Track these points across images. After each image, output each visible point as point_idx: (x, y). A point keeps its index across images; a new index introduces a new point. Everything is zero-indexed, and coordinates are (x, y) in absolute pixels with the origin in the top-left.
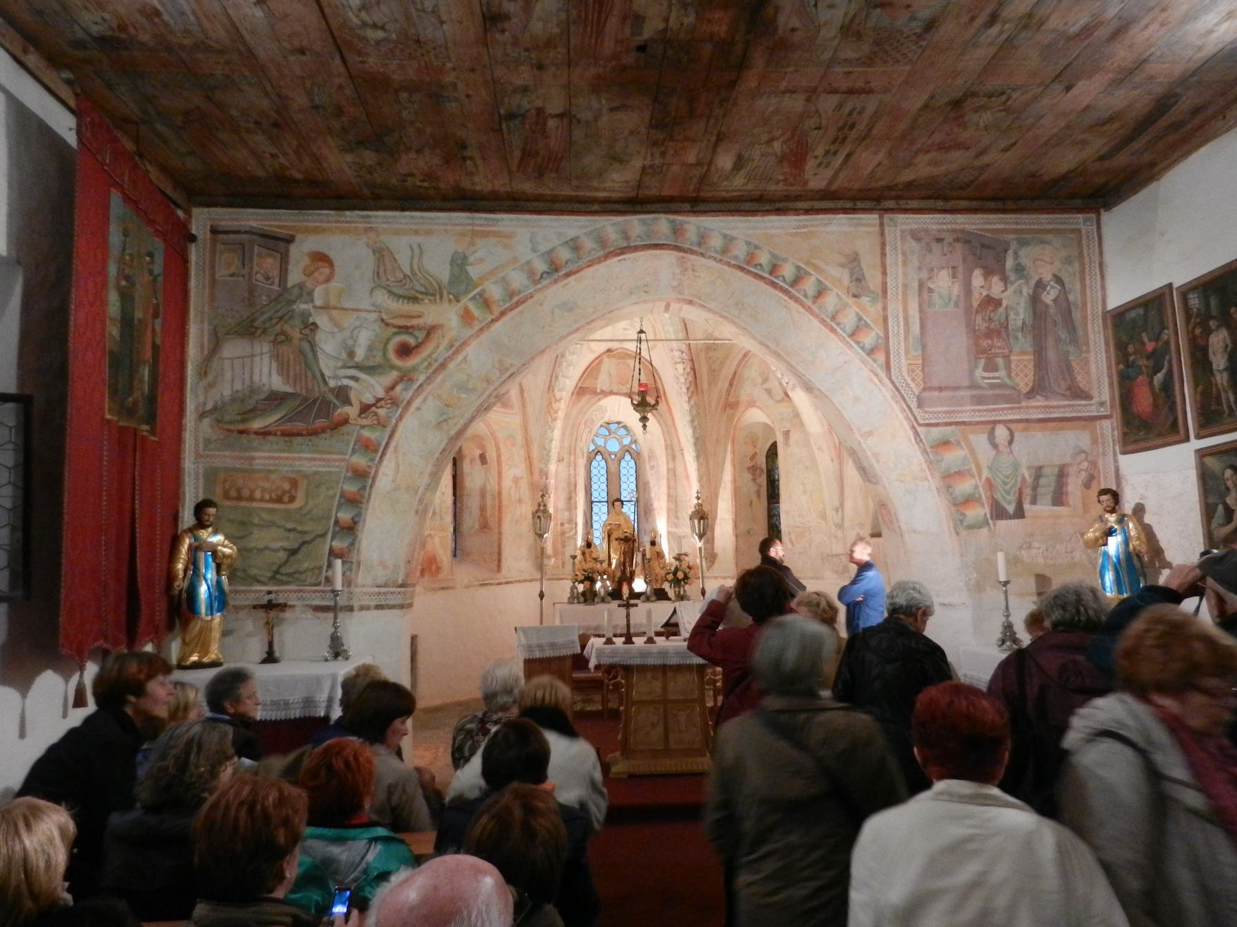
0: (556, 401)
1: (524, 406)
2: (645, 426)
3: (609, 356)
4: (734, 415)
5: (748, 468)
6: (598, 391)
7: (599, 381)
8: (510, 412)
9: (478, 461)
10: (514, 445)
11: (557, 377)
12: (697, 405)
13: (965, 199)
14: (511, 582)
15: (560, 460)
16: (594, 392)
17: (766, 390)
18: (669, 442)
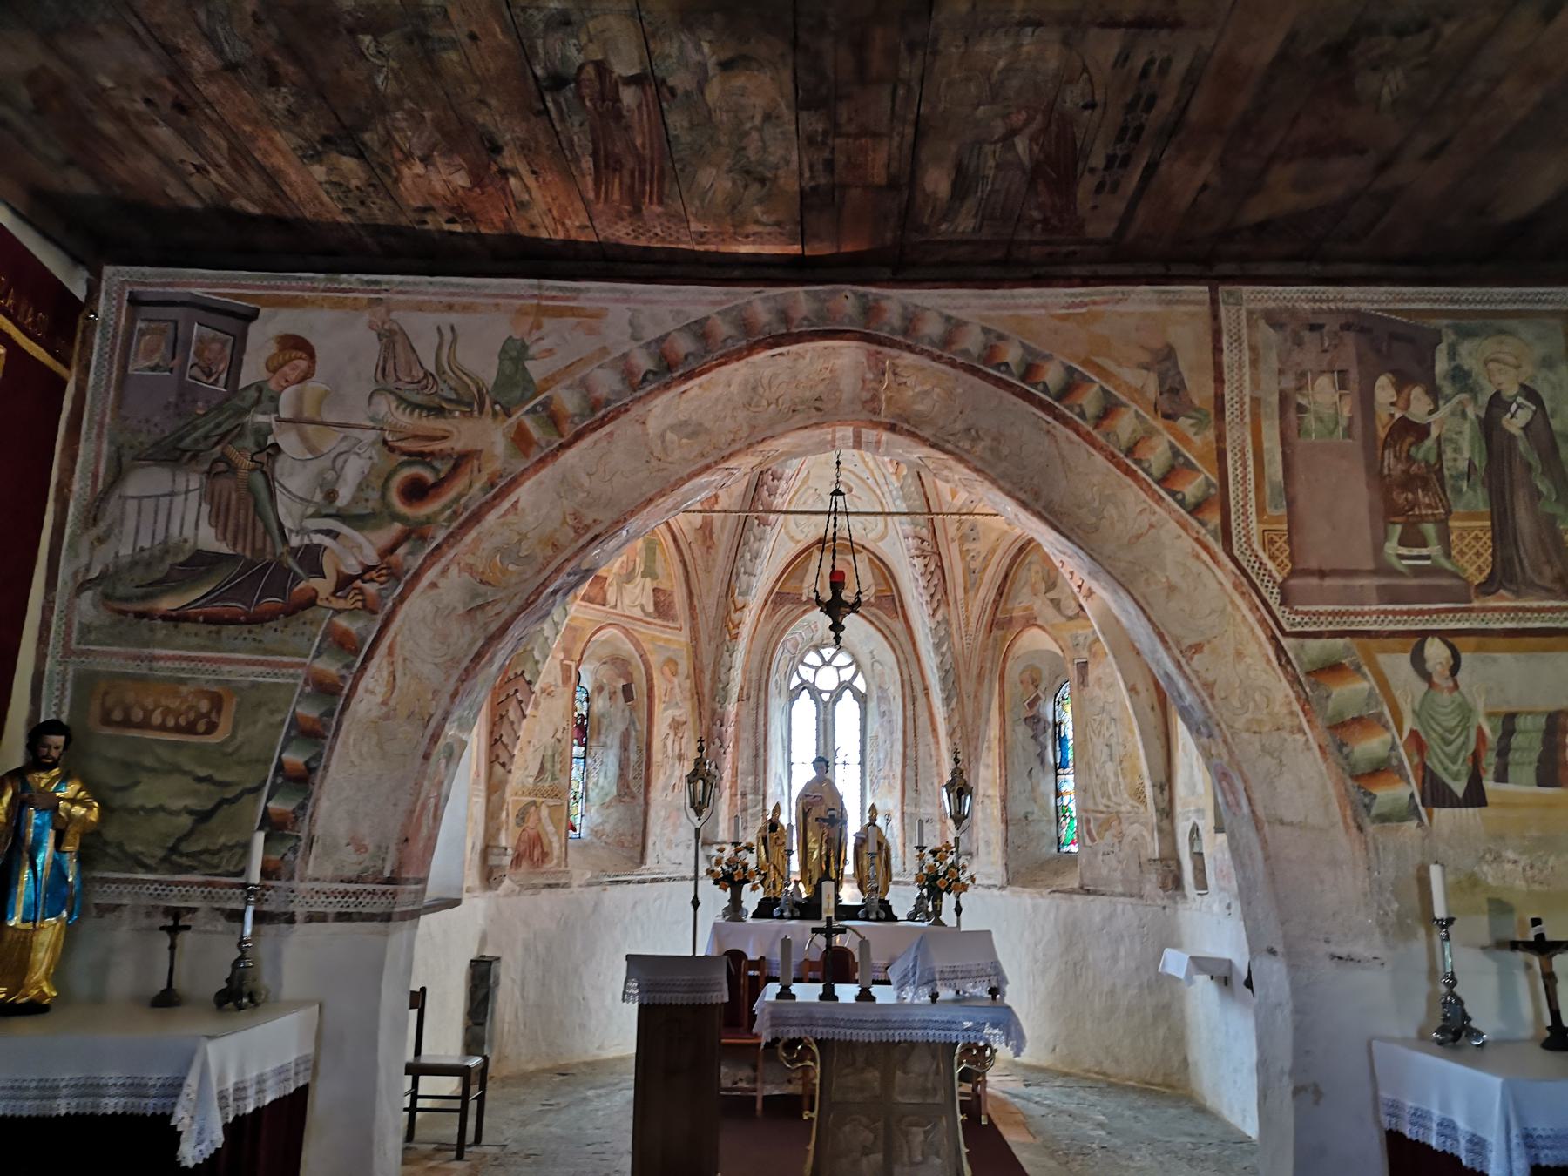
0: (736, 610)
1: (693, 617)
4: (1004, 639)
5: (1026, 719)
6: (804, 599)
8: (671, 625)
10: (674, 674)
17: (1052, 600)
18: (906, 677)
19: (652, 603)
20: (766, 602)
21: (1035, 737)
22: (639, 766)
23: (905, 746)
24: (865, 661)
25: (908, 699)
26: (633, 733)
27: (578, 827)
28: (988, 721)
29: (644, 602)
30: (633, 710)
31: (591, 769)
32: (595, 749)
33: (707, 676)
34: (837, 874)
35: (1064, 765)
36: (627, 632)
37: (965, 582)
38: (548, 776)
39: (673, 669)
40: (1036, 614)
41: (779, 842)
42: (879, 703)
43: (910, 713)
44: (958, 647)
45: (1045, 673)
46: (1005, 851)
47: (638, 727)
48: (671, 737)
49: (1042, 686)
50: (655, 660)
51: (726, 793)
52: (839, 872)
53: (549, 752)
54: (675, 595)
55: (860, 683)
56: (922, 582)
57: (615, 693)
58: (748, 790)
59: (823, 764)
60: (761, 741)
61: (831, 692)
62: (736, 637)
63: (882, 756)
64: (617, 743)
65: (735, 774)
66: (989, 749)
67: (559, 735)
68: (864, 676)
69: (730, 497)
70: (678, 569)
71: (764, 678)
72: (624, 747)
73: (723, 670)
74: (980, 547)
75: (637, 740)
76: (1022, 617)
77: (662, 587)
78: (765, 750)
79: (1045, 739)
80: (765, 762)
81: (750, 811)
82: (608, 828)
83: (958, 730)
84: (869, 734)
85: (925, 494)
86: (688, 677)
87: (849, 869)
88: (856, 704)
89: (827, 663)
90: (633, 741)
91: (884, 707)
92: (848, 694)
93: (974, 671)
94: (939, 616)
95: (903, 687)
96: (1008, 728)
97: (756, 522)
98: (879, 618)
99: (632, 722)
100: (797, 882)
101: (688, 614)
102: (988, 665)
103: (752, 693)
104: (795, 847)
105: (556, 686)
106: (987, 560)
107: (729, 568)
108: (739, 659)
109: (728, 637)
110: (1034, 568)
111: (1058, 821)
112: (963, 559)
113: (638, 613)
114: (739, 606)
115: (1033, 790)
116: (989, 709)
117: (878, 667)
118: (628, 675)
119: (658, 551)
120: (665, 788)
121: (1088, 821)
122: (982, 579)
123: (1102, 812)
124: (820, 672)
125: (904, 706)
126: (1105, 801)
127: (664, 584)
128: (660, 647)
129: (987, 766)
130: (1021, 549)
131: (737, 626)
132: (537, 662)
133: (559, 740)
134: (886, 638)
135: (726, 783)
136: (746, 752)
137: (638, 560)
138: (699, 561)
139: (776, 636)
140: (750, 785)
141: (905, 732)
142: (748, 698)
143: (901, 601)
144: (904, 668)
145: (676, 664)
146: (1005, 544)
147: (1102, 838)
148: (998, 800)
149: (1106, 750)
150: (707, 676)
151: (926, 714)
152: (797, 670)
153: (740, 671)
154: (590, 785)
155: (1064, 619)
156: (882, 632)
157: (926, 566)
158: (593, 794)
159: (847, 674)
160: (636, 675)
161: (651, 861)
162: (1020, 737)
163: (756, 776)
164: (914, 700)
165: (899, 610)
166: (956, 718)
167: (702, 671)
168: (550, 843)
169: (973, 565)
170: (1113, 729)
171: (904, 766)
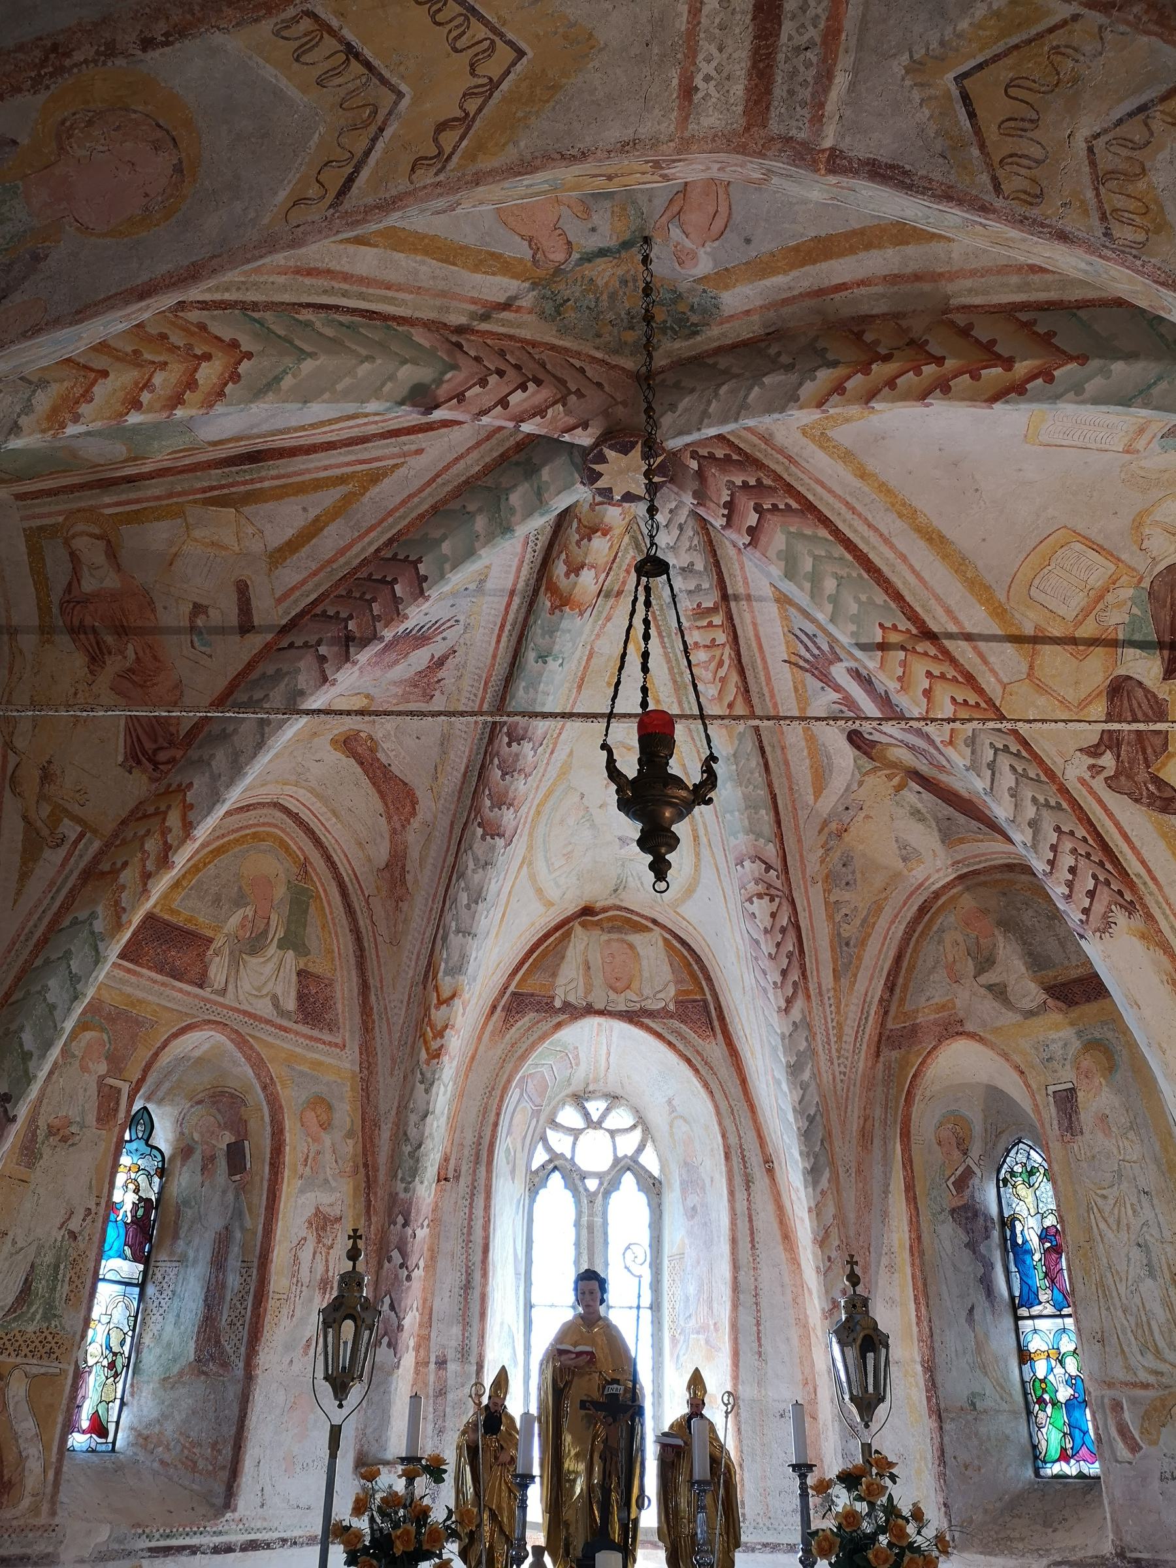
0: (441, 1002)
1: (367, 1028)
2: (660, 869)
3: (583, 925)
4: (904, 1064)
5: (953, 1211)
6: (558, 1004)
7: (561, 980)
8: (326, 1037)
9: (222, 1164)
10: (325, 1126)
11: (445, 938)
12: (805, 1025)
13: (1170, 922)
14: (268, 1546)
15: (442, 1178)
16: (546, 1006)
17: (990, 988)
18: (733, 1140)
19: (293, 994)
20: (494, 1008)
21: (972, 1246)
22: (242, 1300)
23: (736, 1267)
24: (658, 1118)
25: (738, 1180)
26: (238, 1235)
27: (112, 1428)
28: (885, 1214)
29: (279, 991)
30: (242, 1189)
31: (151, 1306)
32: (164, 1266)
33: (385, 1133)
34: (625, 1528)
35: (1029, 1298)
36: (241, 1042)
37: (835, 961)
38: (37, 1308)
39: (324, 1117)
40: (961, 1014)
41: (504, 1458)
42: (684, 1191)
43: (741, 1206)
44: (826, 1078)
45: (978, 1128)
46: (942, 1476)
47: (248, 1223)
48: (310, 1246)
49: (976, 1150)
50: (292, 1097)
51: (408, 1360)
52: (630, 1528)
53: (49, 1259)
54: (338, 988)
55: (650, 1161)
56: (767, 947)
57: (213, 1158)
58: (451, 1354)
59: (595, 1284)
60: (477, 1257)
61: (600, 1176)
62: (436, 1055)
63: (692, 1290)
64: (205, 1255)
65: (428, 1320)
66: (891, 1267)
67: (74, 1225)
68: (656, 1149)
69: (436, 800)
70: (344, 943)
71: (485, 1143)
72: (218, 1262)
73: (413, 1118)
74: (856, 899)
75: (244, 1247)
76: (935, 1023)
77: (312, 969)
78: (485, 1275)
79: (989, 1249)
80: (483, 1298)
81: (451, 1396)
82: (170, 1428)
83: (834, 1232)
84: (667, 1249)
85: (770, 785)
86: (350, 1134)
87: (649, 1518)
88: (642, 1199)
89: (593, 1124)
90: (235, 1250)
91: (693, 1199)
92: (628, 1179)
93: (854, 1125)
94: (796, 1013)
95: (727, 1157)
96: (924, 1226)
97: (480, 831)
98: (683, 1038)
99: (238, 1214)
100: (538, 1551)
101: (357, 1019)
102: (878, 1112)
103: (464, 1168)
104: (536, 1471)
105: (82, 1126)
106: (867, 925)
107: (429, 932)
108: (443, 1097)
109: (424, 1055)
110: (948, 938)
111: (1029, 1412)
112: (830, 917)
113: (264, 1008)
114: (446, 994)
115: (980, 1348)
116: (886, 1192)
117: (682, 1128)
118: (240, 1127)
119: (312, 910)
120: (288, 1348)
121: (1117, 1407)
122: (860, 958)
123: (1146, 1386)
124: (581, 1137)
125: (731, 1193)
126: (1150, 1361)
127: (319, 967)
128: (302, 1074)
129: (891, 1302)
130: (923, 910)
131: (440, 1034)
132: (27, 1056)
133: (73, 1236)
134: (696, 1071)
135: (409, 1338)
136: (450, 1278)
137: (274, 917)
138: (382, 928)
139: (509, 1067)
140: (454, 1343)
141: (734, 1241)
142: (457, 1178)
143: (719, 1008)
144: (728, 1122)
145: (330, 1107)
146: (897, 897)
147: (1154, 1443)
148: (919, 1368)
149: (1136, 1253)
150: (385, 1133)
151: (771, 1208)
152: (544, 1139)
153: (443, 1120)
154: (147, 1340)
155: (1018, 1017)
156: (689, 1061)
157: (773, 915)
158: (149, 1359)
159: (628, 1144)
160: (253, 1125)
161: (246, 1501)
162: (947, 1244)
163: (466, 1324)
164: (748, 1182)
165: (716, 1023)
166: (831, 1210)
167: (376, 1125)
168: (21, 1459)
169: (847, 931)
170: (1147, 1213)
171: (735, 1306)
